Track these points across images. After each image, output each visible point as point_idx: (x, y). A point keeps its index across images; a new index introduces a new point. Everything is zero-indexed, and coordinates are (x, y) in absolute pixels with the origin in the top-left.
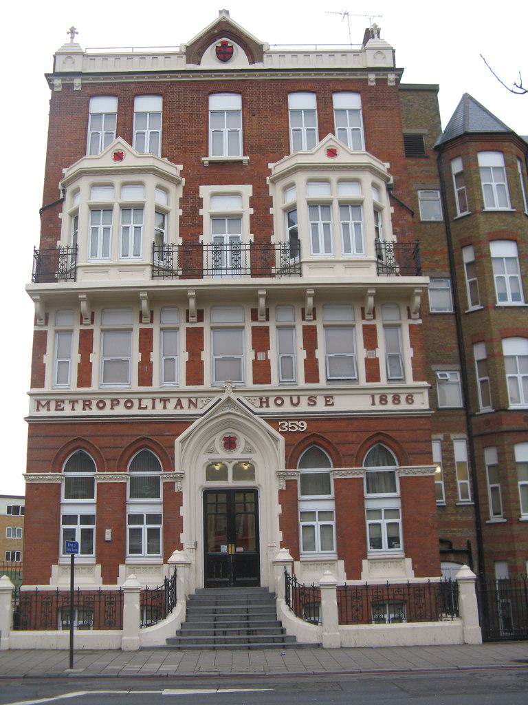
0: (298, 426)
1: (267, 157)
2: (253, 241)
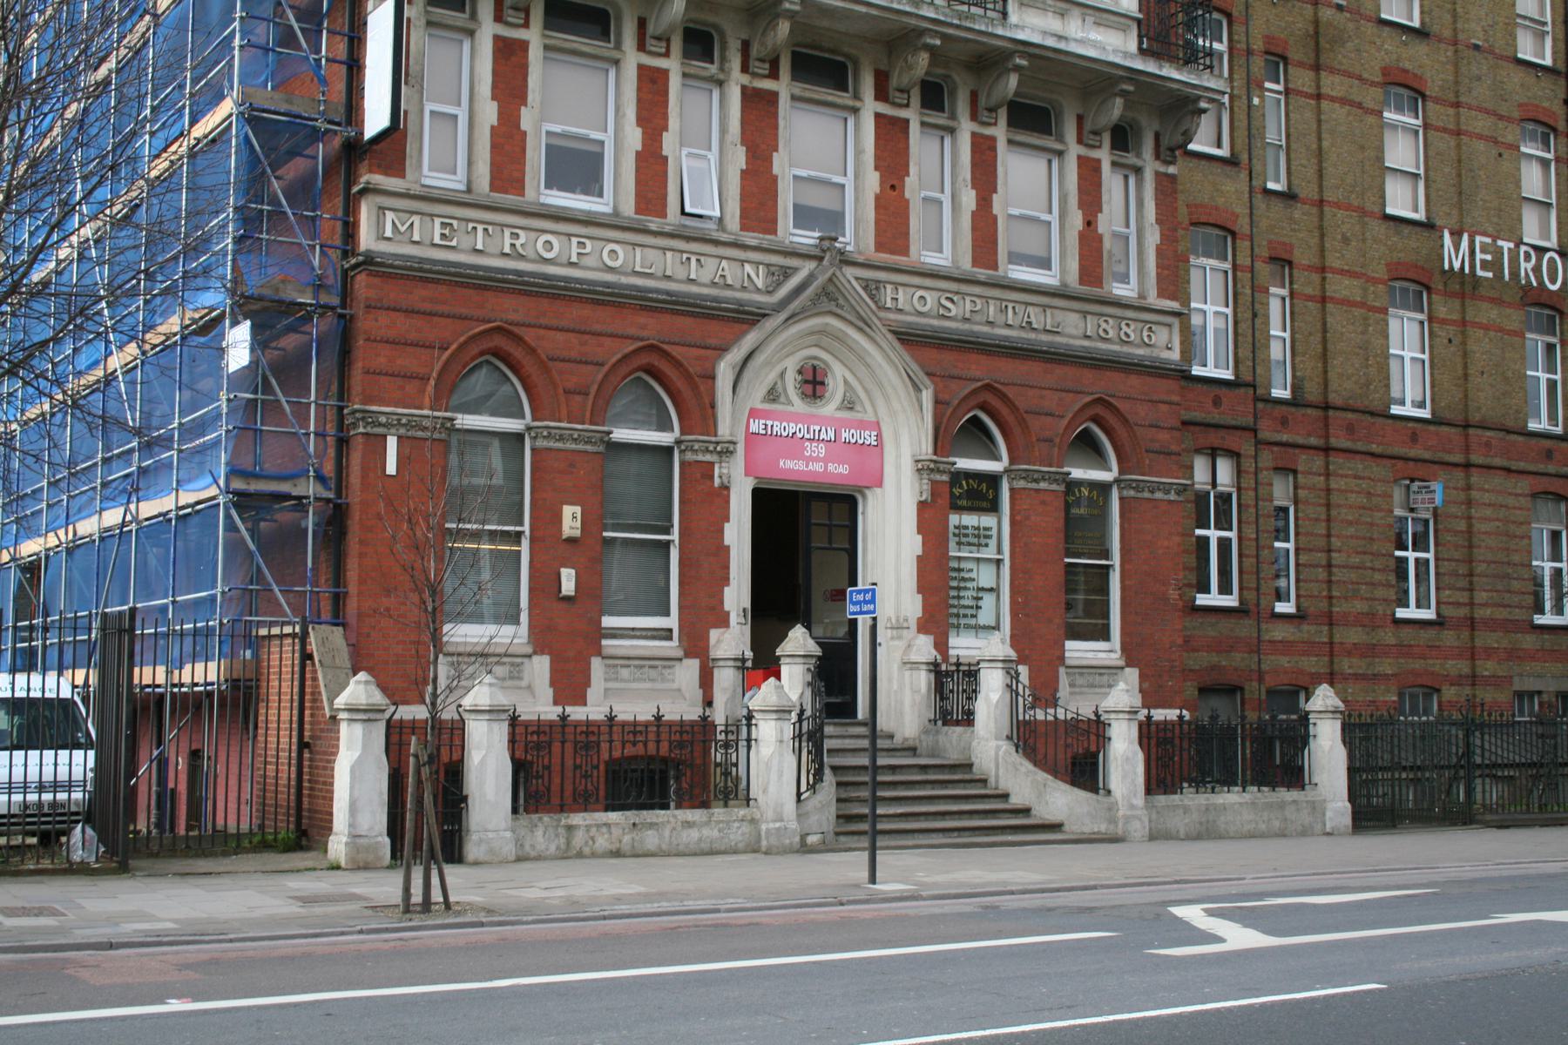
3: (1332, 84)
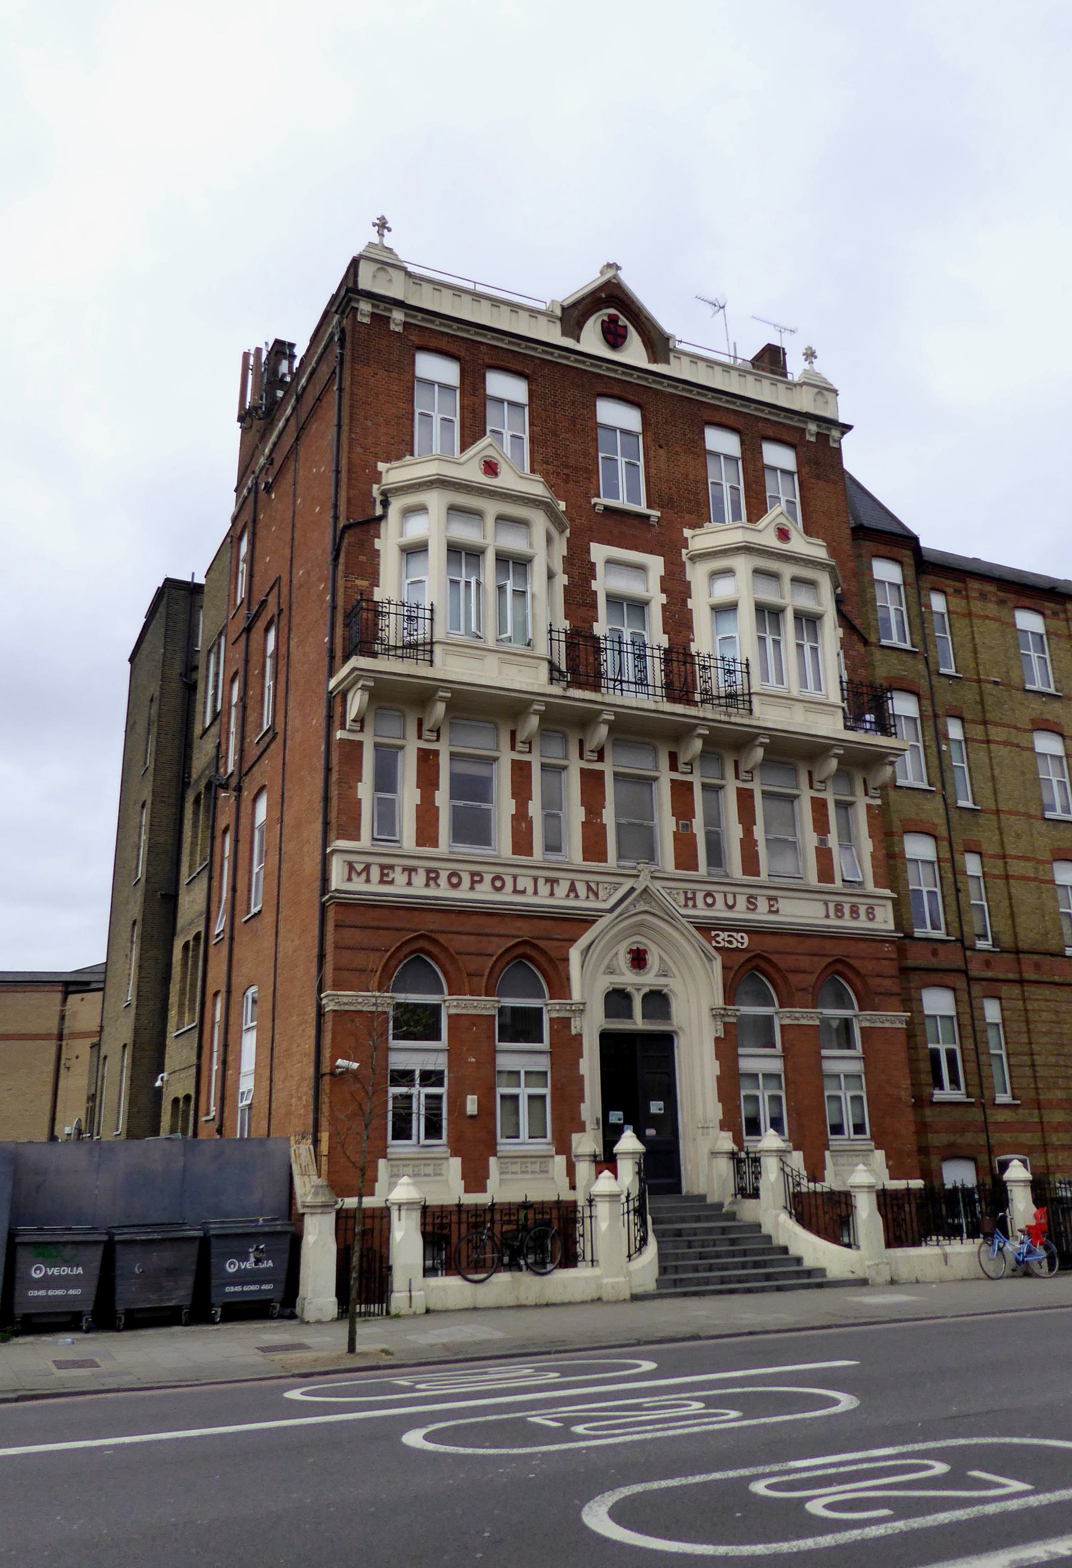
1: (680, 517)
3: (997, 733)
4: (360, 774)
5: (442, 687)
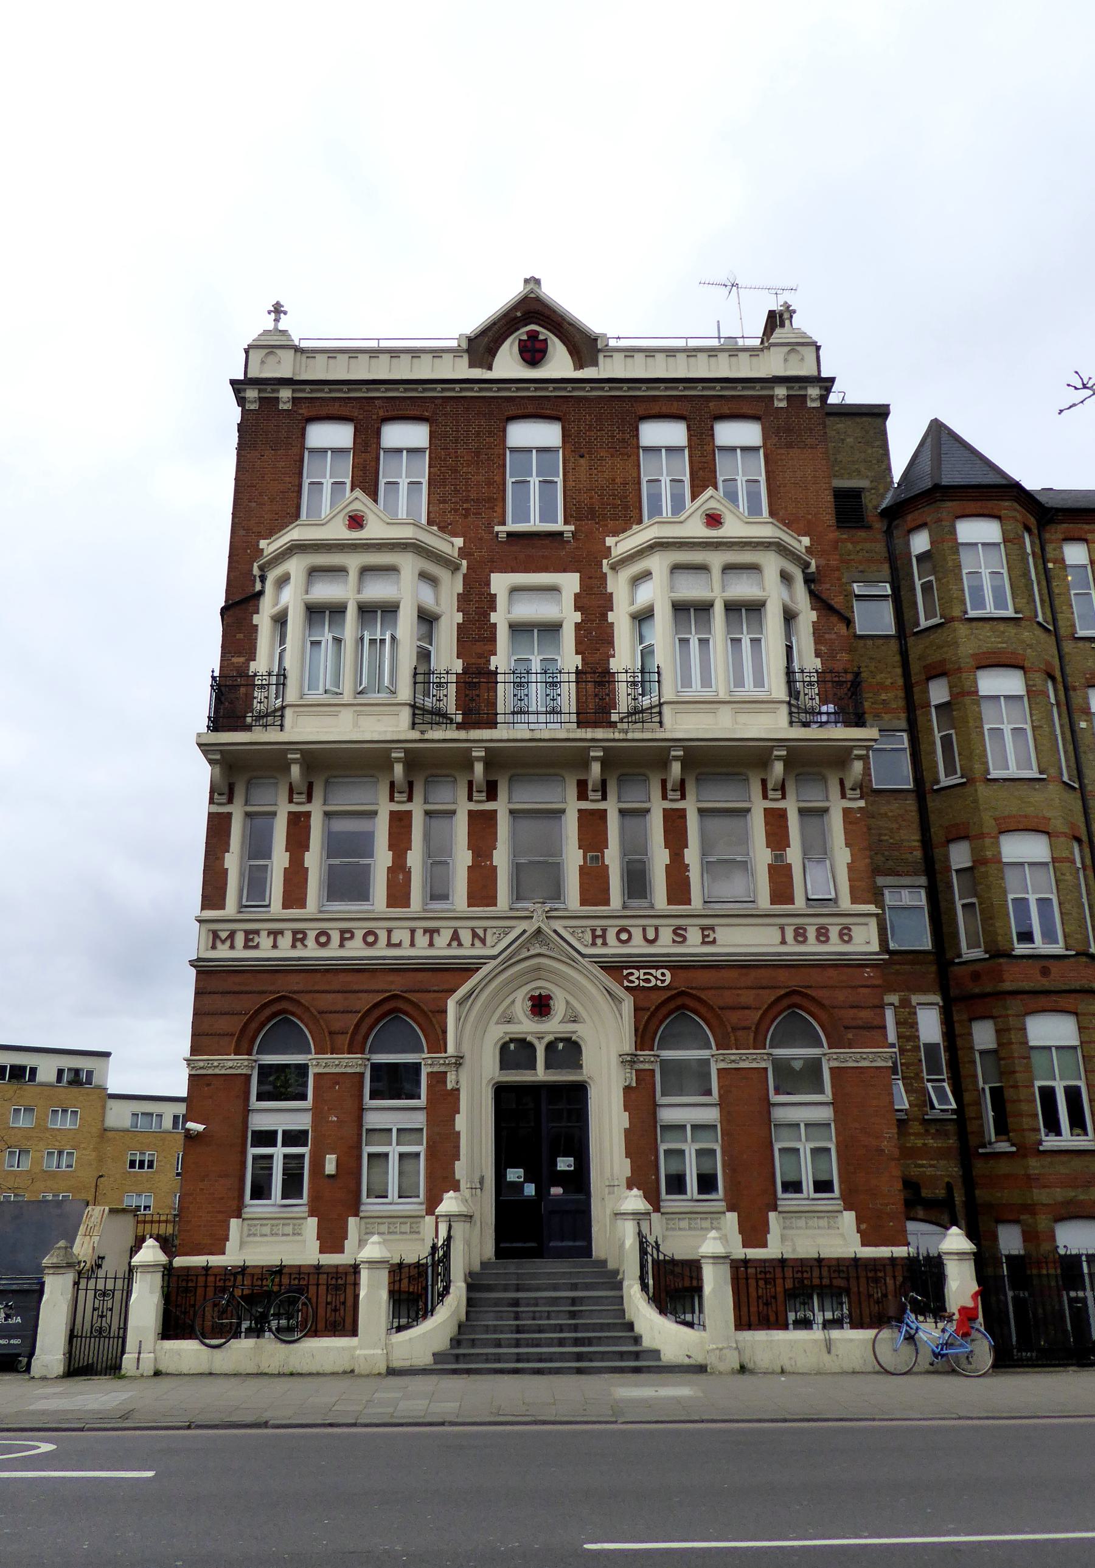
0: (656, 977)
2: (580, 668)
4: (228, 844)
5: (594, 747)
